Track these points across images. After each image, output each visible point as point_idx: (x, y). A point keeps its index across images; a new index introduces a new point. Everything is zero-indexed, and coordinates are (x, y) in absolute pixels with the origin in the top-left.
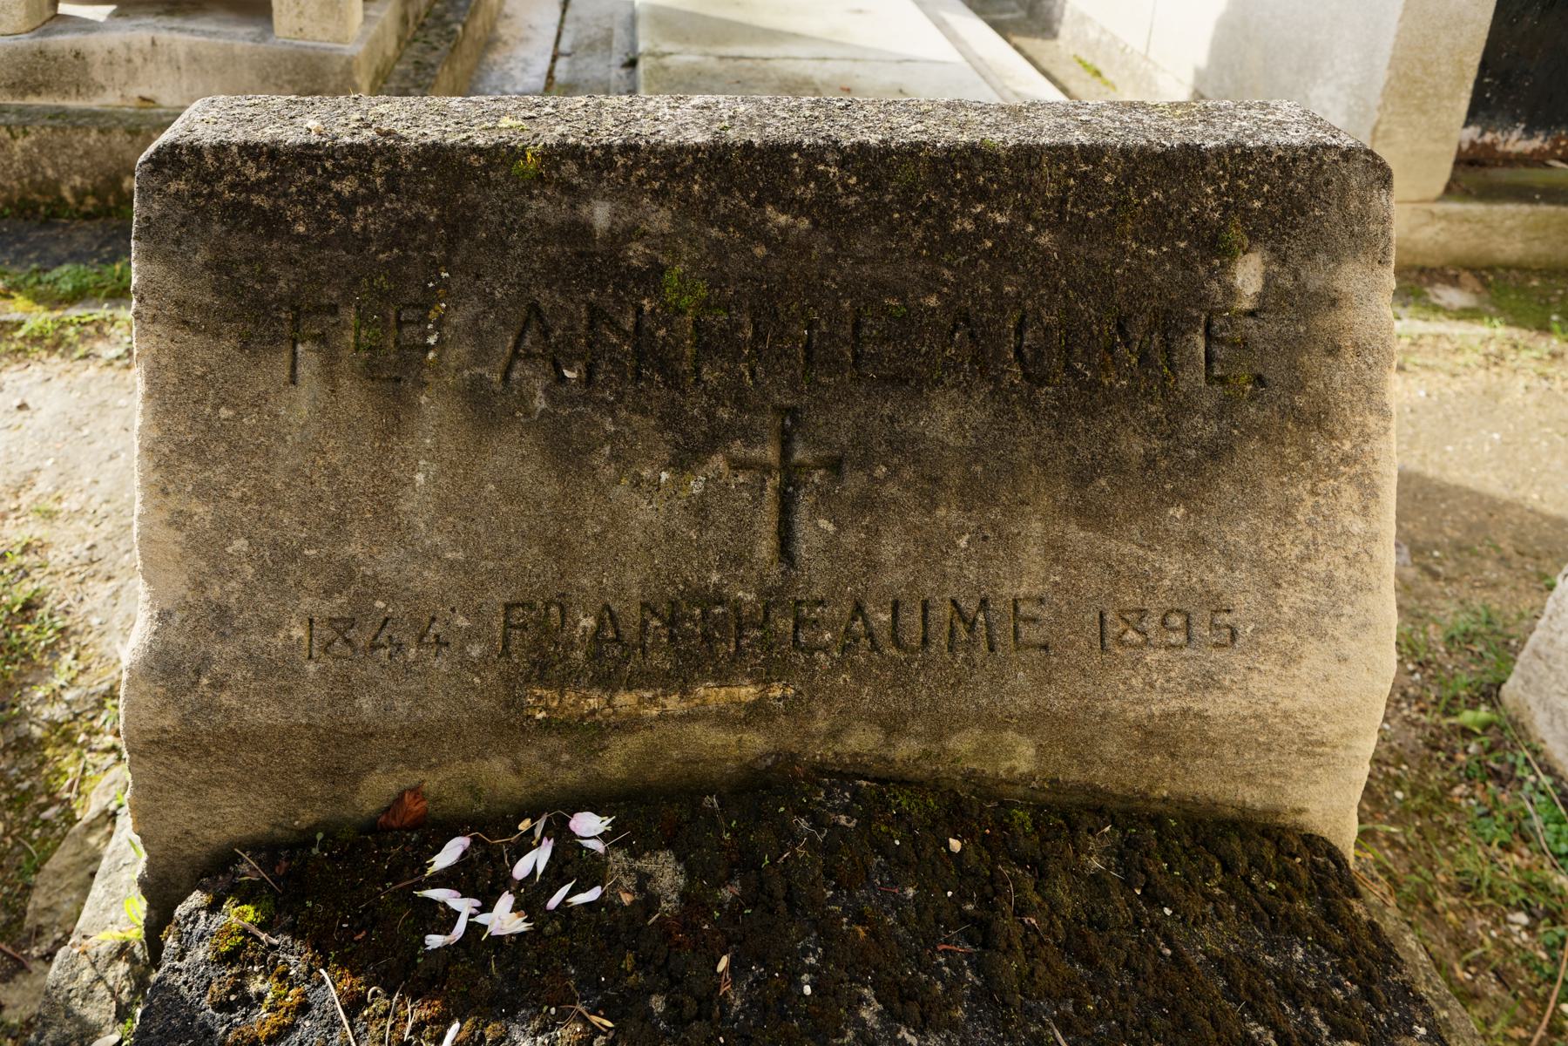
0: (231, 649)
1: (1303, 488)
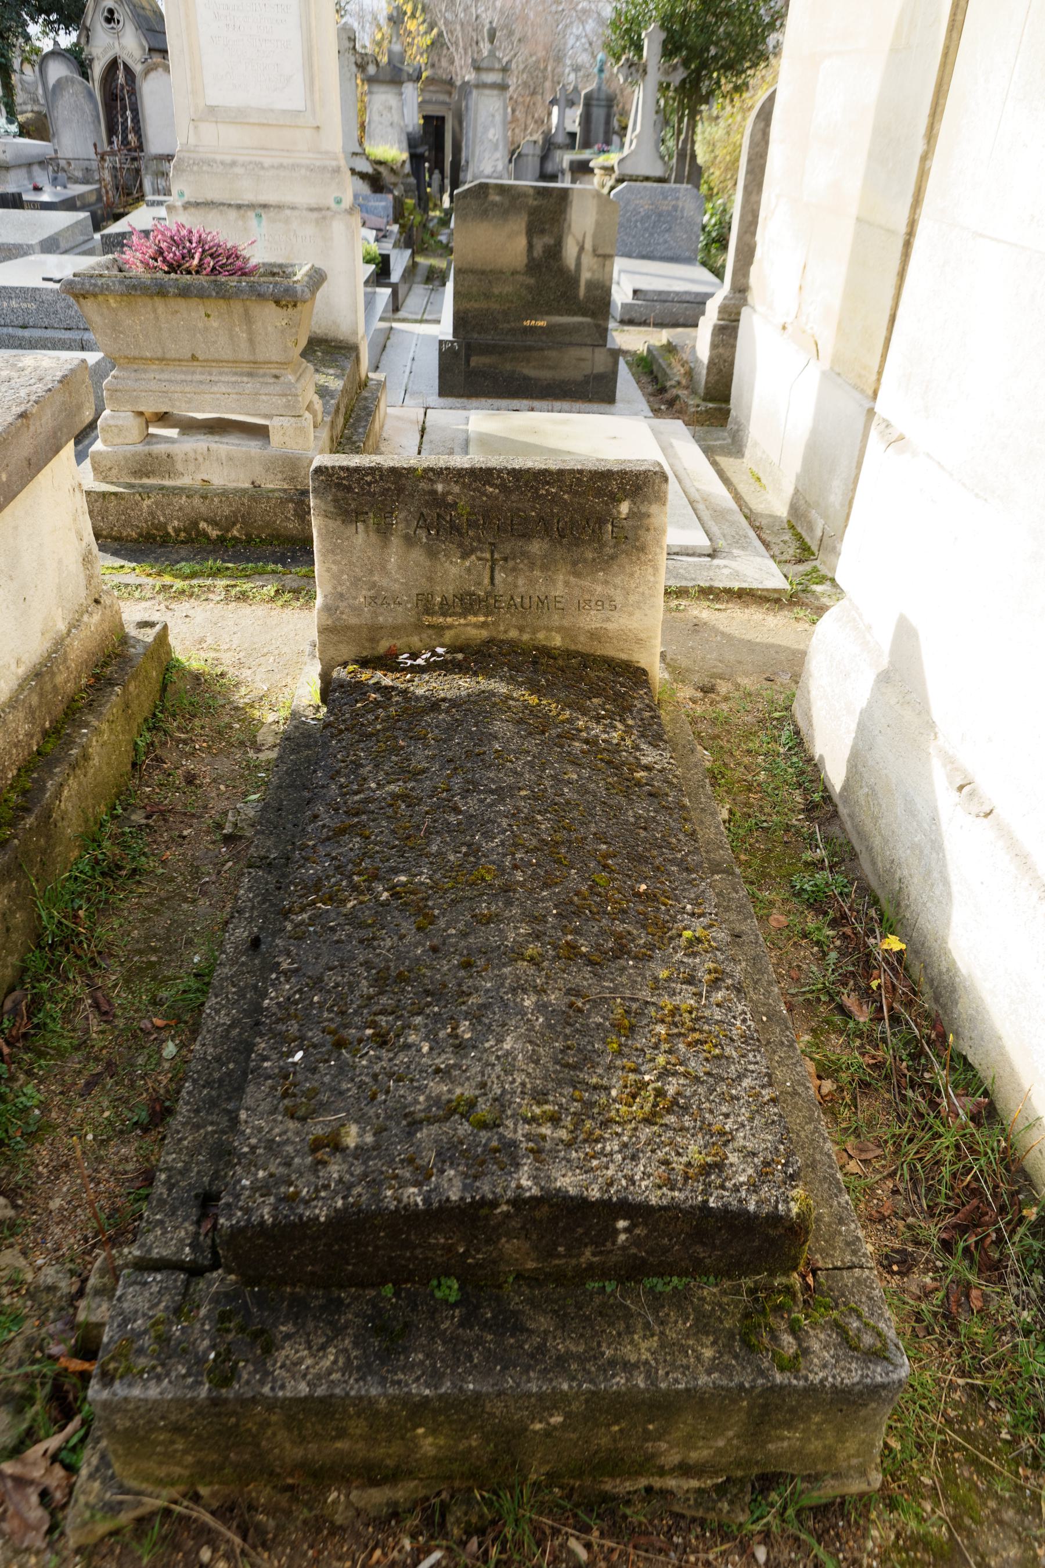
0: (345, 604)
1: (637, 568)
